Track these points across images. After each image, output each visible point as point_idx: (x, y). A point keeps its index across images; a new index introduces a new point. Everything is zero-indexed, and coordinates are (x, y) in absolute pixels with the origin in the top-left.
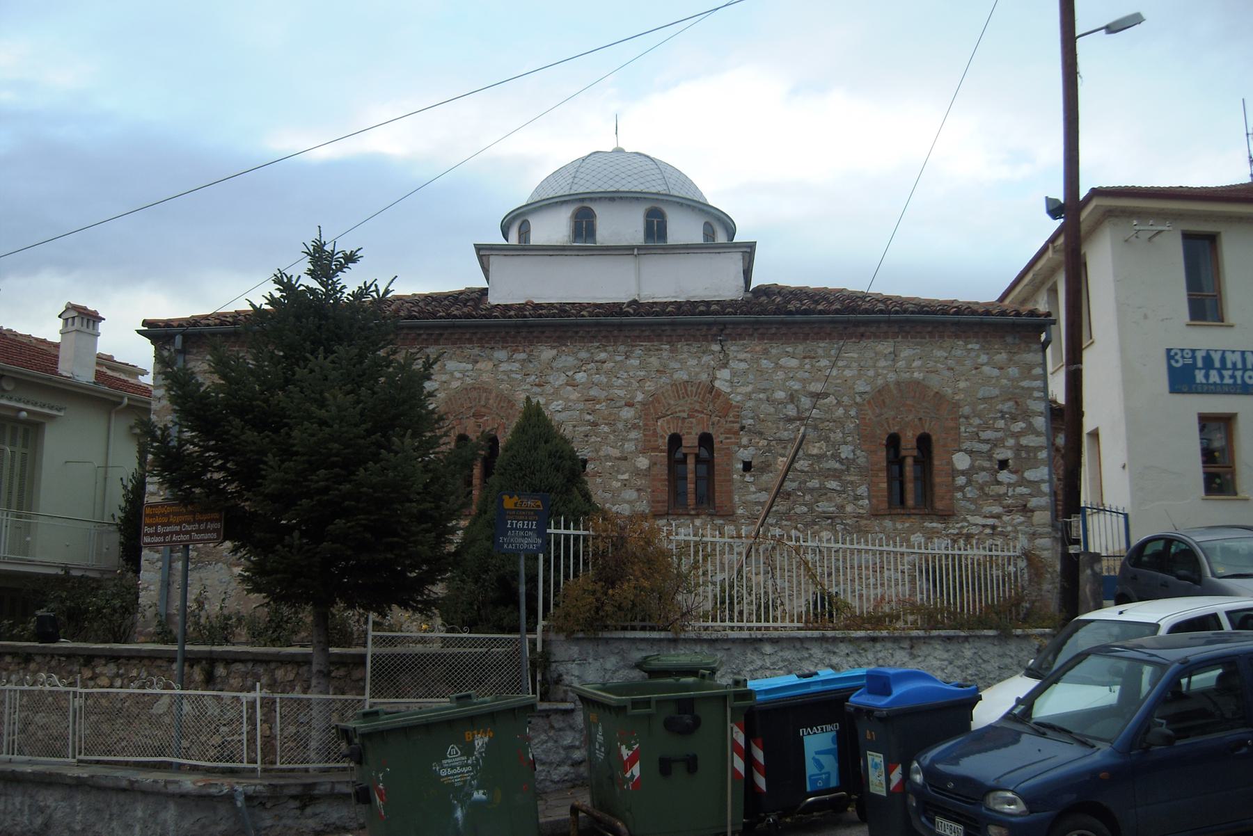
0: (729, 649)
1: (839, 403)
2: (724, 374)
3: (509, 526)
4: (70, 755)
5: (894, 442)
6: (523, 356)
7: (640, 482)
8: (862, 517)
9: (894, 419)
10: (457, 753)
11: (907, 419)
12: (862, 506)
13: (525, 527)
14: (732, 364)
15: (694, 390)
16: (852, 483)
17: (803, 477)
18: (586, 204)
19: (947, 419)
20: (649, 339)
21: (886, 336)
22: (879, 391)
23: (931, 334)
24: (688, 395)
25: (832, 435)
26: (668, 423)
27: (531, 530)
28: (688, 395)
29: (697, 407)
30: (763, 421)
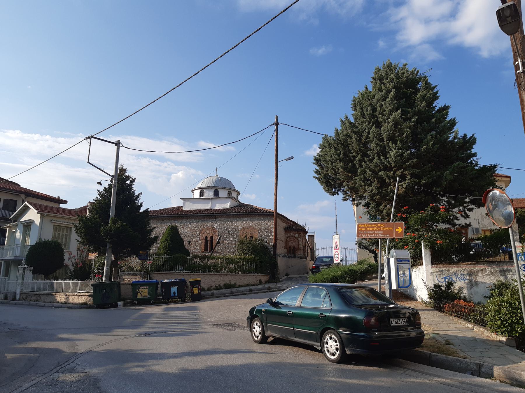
1: (236, 230)
2: (216, 225)
6: (180, 222)
14: (217, 223)
20: (203, 218)
21: (245, 217)
23: (254, 217)
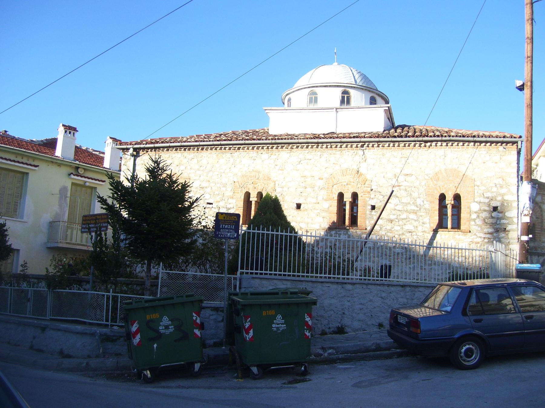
0: (329, 287)
3: (221, 227)
4: (8, 311)
5: (442, 197)
7: (324, 214)
8: (426, 232)
9: (443, 186)
10: (167, 320)
11: (449, 187)
12: (426, 227)
13: (229, 228)
15: (350, 172)
16: (421, 216)
17: (399, 213)
18: (347, 89)
19: (468, 187)
22: (436, 173)
24: (347, 175)
25: (413, 194)
26: (338, 187)
27: (232, 229)
28: (347, 175)
29: (352, 180)
30: (381, 187)
